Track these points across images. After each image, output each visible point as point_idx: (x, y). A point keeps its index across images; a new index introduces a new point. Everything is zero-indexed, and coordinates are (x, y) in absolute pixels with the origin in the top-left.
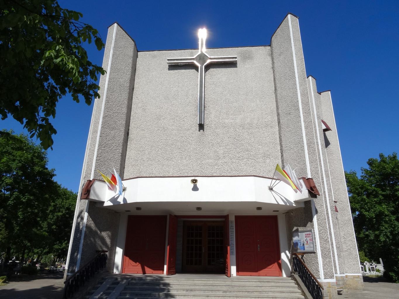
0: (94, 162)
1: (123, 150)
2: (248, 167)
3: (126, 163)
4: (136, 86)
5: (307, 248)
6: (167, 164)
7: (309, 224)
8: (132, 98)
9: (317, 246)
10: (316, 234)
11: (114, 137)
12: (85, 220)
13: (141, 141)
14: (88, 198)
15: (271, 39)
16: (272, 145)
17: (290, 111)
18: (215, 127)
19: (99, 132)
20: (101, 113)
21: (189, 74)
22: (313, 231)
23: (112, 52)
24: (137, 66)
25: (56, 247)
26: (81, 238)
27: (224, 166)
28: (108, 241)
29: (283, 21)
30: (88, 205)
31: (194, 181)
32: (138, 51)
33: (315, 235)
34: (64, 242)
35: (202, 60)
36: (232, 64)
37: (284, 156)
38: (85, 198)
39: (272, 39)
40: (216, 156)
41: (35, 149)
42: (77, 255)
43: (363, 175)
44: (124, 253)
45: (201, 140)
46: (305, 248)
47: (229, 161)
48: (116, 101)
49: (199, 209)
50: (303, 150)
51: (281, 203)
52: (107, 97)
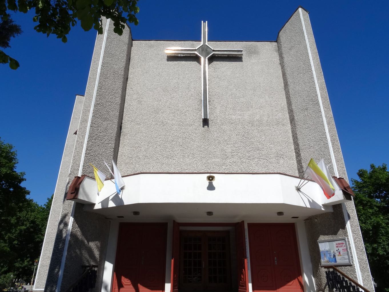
0: (82, 156)
1: (115, 145)
2: (260, 168)
3: (118, 161)
4: (130, 76)
5: (340, 259)
6: (167, 162)
7: (341, 231)
8: (126, 89)
9: (354, 258)
10: (351, 244)
11: (106, 129)
12: (70, 226)
13: (136, 136)
14: (76, 198)
15: (279, 34)
16: (284, 144)
17: (307, 107)
18: (221, 123)
19: (89, 121)
20: (92, 100)
21: (190, 66)
22: (346, 240)
23: (106, 34)
24: (131, 55)
25: (17, 265)
26: (64, 250)
27: (232, 166)
28: (97, 253)
29: (293, 14)
30: (74, 208)
31: (211, 179)
32: (133, 40)
33: (349, 244)
34: (26, 260)
35: (205, 52)
36: (236, 58)
37: (302, 156)
38: (72, 198)
39: (280, 34)
40: (223, 155)
41: (4, 148)
42: (59, 271)
43: (354, 186)
44: (114, 270)
45: (206, 137)
46: (337, 260)
47: (238, 161)
48: (110, 89)
49: (210, 213)
50: (327, 148)
51: (308, 206)
52: (99, 83)
